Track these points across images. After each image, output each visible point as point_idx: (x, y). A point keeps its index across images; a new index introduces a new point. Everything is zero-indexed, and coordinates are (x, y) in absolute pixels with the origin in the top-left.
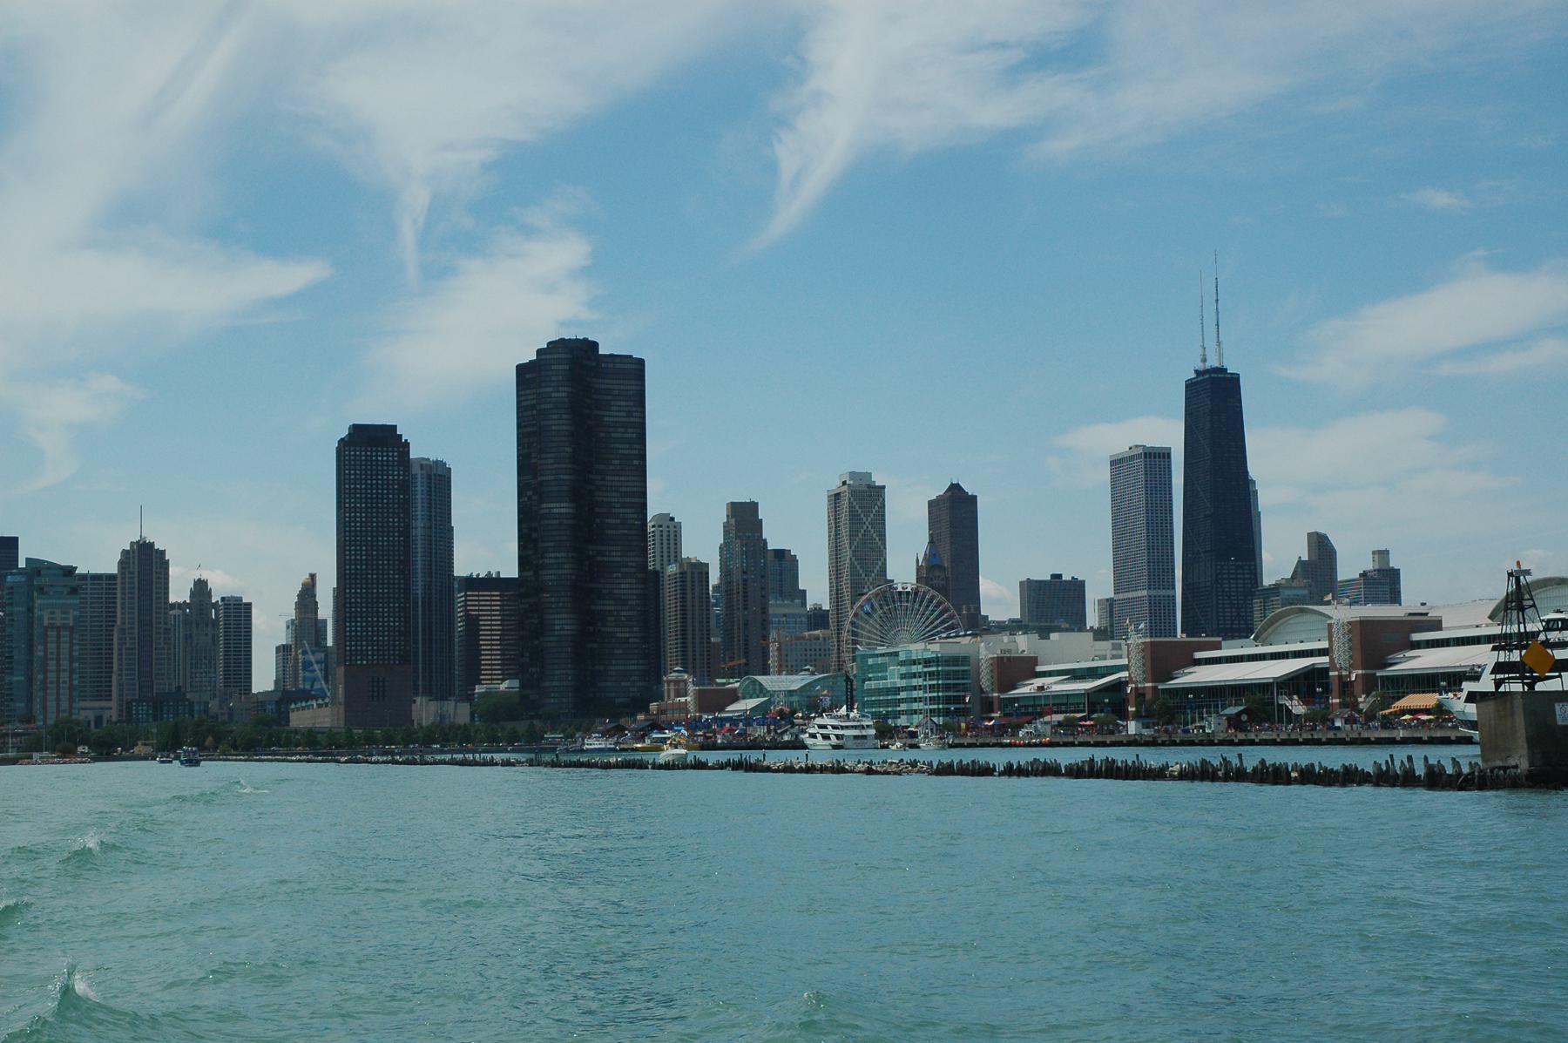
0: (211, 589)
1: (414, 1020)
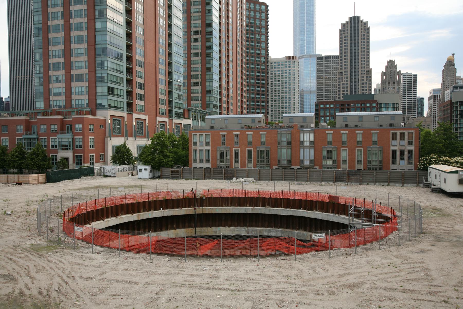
0: (396, 65)
1: (98, 267)
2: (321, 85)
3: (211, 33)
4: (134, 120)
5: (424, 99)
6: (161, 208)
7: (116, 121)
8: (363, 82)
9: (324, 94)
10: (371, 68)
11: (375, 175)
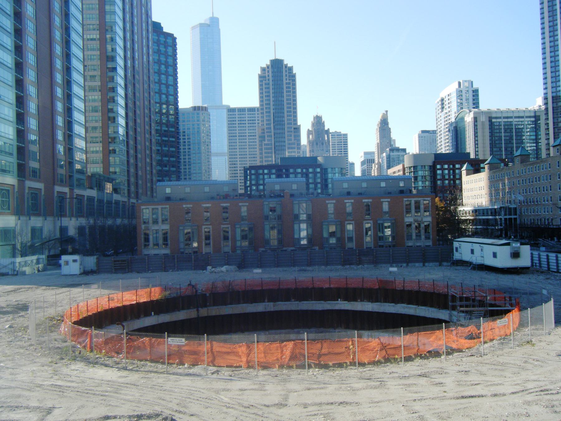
0: (324, 122)
2: (234, 146)
3: (114, 69)
4: (27, 191)
6: (153, 313)
7: (4, 191)
8: (290, 142)
9: (238, 156)
10: (299, 124)
11: (391, 253)
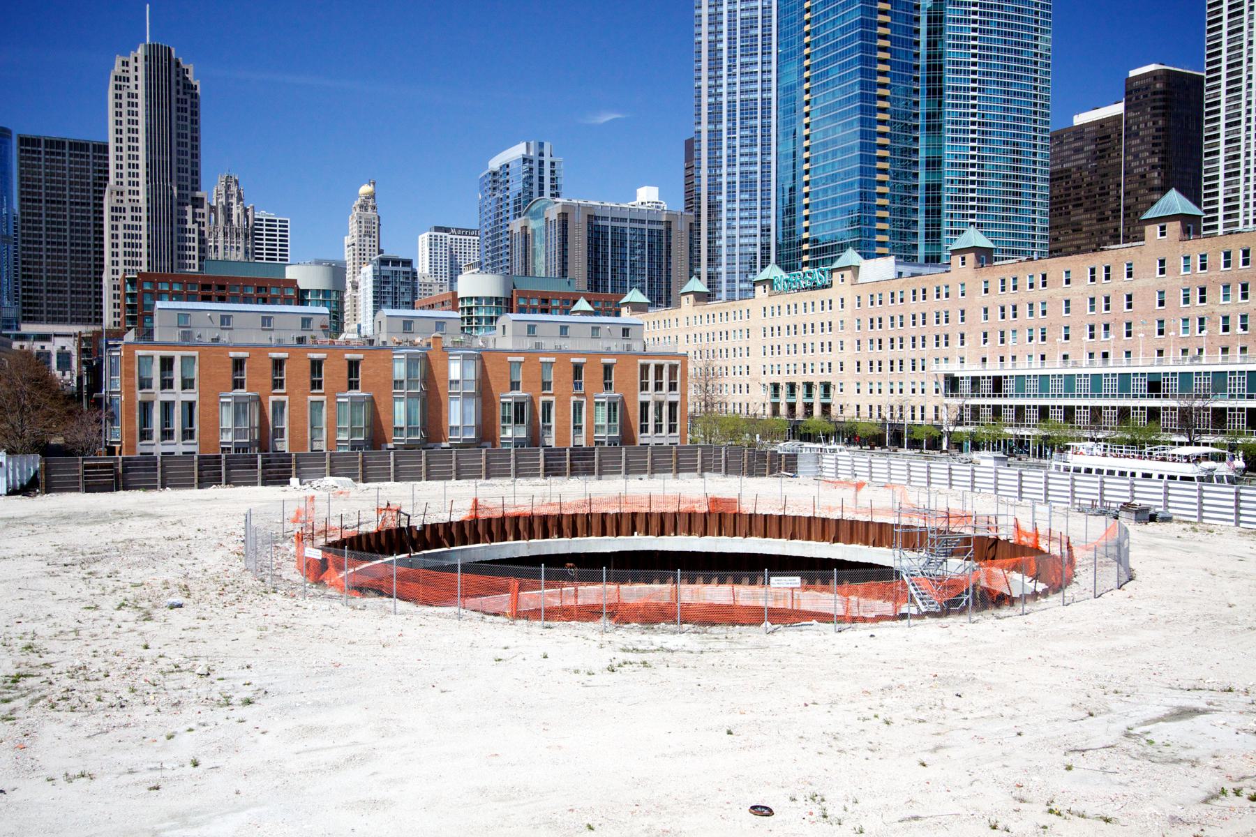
5: (296, 281)
